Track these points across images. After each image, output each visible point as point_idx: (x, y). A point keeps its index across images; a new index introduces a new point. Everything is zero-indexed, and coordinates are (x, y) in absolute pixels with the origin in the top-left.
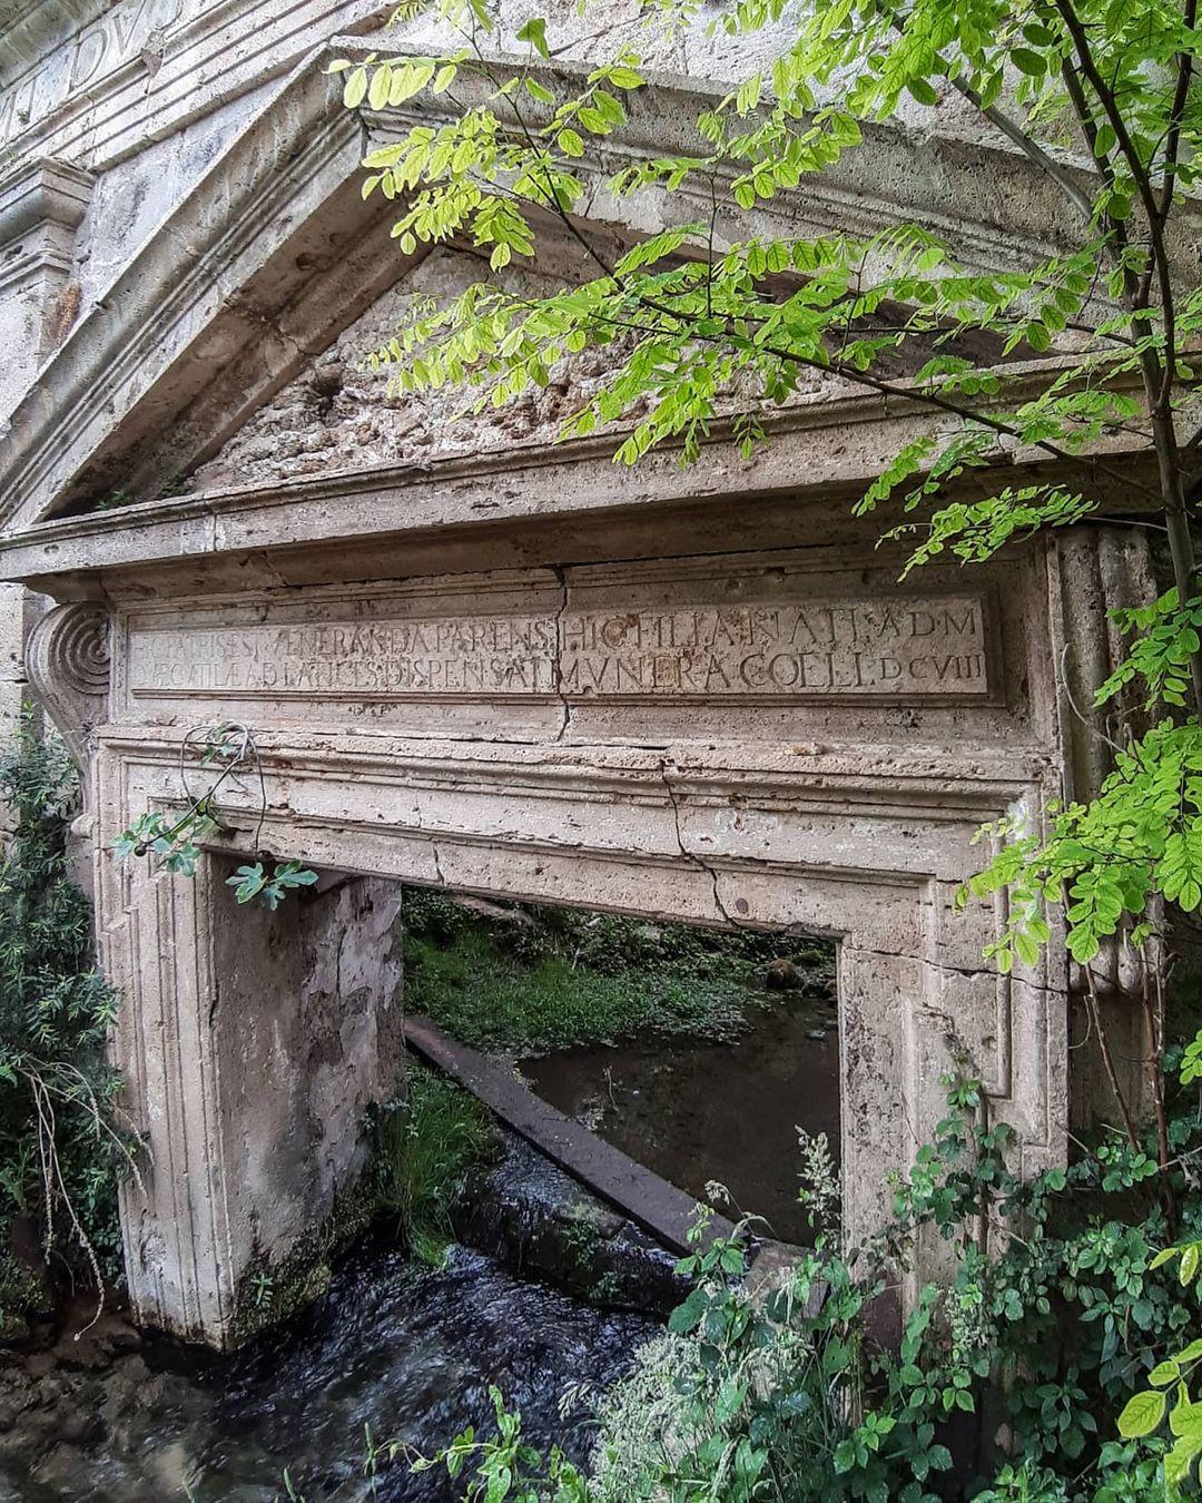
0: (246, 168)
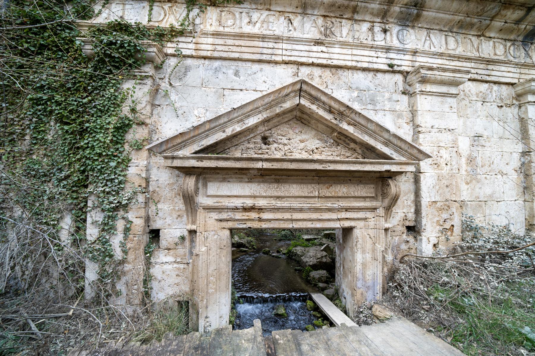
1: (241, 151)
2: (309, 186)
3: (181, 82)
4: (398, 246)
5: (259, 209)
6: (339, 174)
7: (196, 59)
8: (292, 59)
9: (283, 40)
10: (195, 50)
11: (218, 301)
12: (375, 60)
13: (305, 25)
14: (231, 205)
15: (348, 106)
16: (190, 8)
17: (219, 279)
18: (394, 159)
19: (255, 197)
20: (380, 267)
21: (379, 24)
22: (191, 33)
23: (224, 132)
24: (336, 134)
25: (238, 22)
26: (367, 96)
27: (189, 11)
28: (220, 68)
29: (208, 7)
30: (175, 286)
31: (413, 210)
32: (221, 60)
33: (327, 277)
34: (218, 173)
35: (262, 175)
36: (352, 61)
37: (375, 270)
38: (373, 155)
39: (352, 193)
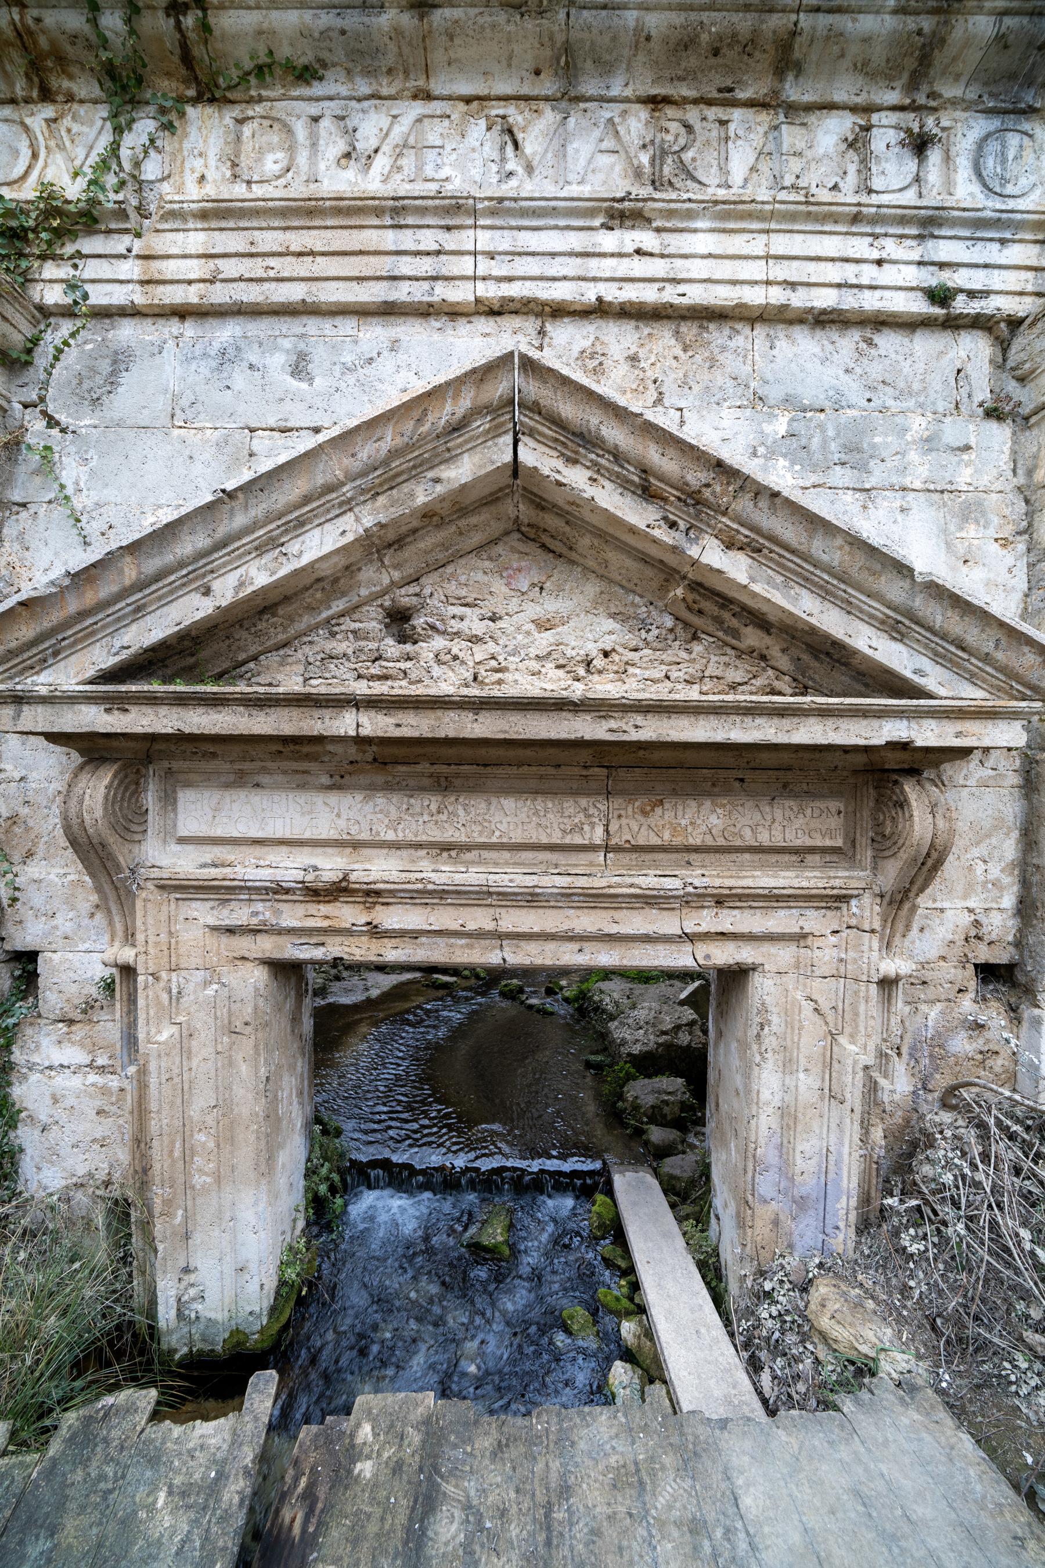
0: (412, 423)
1: (301, 668)
2: (569, 805)
3: (98, 413)
4: (938, 1042)
5: (368, 893)
6: (689, 756)
7: (150, 321)
8: (515, 290)
9: (475, 213)
10: (143, 283)
11: (228, 1215)
12: (868, 274)
13: (570, 149)
14: (262, 875)
15: (719, 464)
16: (122, 120)
17: (232, 1140)
18: (930, 696)
19: (356, 845)
20: (853, 1131)
21: (893, 118)
22: (121, 214)
23: (207, 592)
24: (680, 592)
25: (302, 158)
26: (831, 433)
27: (118, 130)
28: (238, 349)
29: (190, 110)
30: (96, 1147)
31: (1009, 901)
32: (241, 319)
33: (684, 1106)
34: (214, 755)
35: (381, 763)
36: (768, 283)
37: (833, 1139)
38: (843, 679)
39: (747, 833)
